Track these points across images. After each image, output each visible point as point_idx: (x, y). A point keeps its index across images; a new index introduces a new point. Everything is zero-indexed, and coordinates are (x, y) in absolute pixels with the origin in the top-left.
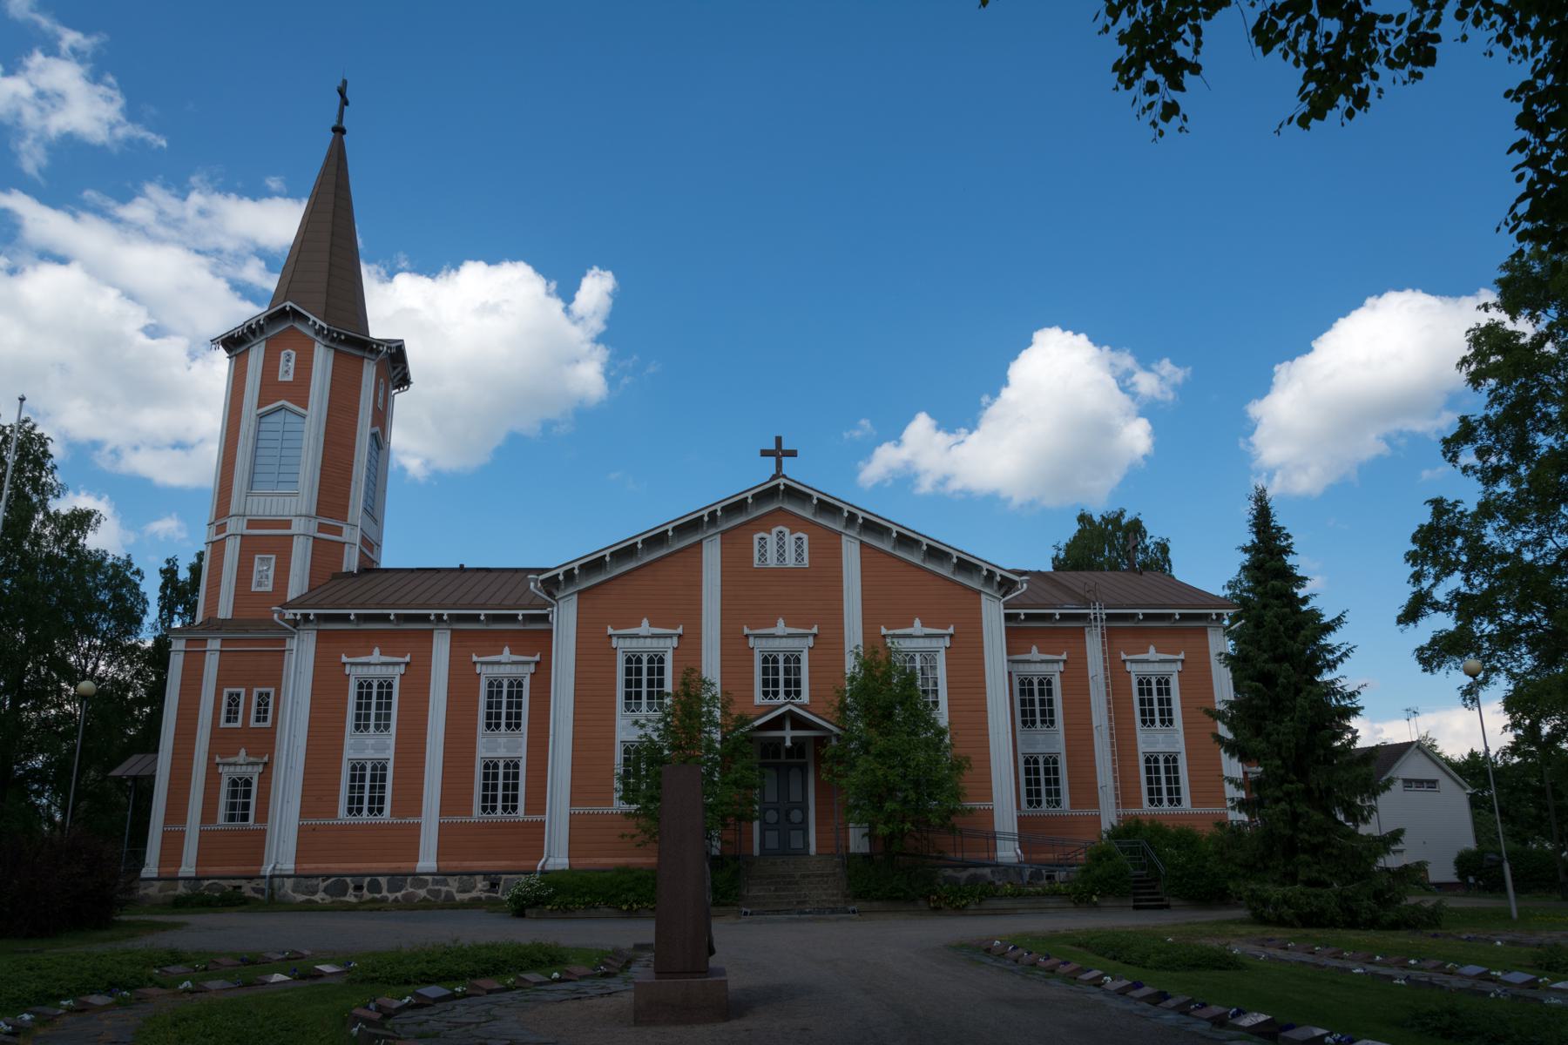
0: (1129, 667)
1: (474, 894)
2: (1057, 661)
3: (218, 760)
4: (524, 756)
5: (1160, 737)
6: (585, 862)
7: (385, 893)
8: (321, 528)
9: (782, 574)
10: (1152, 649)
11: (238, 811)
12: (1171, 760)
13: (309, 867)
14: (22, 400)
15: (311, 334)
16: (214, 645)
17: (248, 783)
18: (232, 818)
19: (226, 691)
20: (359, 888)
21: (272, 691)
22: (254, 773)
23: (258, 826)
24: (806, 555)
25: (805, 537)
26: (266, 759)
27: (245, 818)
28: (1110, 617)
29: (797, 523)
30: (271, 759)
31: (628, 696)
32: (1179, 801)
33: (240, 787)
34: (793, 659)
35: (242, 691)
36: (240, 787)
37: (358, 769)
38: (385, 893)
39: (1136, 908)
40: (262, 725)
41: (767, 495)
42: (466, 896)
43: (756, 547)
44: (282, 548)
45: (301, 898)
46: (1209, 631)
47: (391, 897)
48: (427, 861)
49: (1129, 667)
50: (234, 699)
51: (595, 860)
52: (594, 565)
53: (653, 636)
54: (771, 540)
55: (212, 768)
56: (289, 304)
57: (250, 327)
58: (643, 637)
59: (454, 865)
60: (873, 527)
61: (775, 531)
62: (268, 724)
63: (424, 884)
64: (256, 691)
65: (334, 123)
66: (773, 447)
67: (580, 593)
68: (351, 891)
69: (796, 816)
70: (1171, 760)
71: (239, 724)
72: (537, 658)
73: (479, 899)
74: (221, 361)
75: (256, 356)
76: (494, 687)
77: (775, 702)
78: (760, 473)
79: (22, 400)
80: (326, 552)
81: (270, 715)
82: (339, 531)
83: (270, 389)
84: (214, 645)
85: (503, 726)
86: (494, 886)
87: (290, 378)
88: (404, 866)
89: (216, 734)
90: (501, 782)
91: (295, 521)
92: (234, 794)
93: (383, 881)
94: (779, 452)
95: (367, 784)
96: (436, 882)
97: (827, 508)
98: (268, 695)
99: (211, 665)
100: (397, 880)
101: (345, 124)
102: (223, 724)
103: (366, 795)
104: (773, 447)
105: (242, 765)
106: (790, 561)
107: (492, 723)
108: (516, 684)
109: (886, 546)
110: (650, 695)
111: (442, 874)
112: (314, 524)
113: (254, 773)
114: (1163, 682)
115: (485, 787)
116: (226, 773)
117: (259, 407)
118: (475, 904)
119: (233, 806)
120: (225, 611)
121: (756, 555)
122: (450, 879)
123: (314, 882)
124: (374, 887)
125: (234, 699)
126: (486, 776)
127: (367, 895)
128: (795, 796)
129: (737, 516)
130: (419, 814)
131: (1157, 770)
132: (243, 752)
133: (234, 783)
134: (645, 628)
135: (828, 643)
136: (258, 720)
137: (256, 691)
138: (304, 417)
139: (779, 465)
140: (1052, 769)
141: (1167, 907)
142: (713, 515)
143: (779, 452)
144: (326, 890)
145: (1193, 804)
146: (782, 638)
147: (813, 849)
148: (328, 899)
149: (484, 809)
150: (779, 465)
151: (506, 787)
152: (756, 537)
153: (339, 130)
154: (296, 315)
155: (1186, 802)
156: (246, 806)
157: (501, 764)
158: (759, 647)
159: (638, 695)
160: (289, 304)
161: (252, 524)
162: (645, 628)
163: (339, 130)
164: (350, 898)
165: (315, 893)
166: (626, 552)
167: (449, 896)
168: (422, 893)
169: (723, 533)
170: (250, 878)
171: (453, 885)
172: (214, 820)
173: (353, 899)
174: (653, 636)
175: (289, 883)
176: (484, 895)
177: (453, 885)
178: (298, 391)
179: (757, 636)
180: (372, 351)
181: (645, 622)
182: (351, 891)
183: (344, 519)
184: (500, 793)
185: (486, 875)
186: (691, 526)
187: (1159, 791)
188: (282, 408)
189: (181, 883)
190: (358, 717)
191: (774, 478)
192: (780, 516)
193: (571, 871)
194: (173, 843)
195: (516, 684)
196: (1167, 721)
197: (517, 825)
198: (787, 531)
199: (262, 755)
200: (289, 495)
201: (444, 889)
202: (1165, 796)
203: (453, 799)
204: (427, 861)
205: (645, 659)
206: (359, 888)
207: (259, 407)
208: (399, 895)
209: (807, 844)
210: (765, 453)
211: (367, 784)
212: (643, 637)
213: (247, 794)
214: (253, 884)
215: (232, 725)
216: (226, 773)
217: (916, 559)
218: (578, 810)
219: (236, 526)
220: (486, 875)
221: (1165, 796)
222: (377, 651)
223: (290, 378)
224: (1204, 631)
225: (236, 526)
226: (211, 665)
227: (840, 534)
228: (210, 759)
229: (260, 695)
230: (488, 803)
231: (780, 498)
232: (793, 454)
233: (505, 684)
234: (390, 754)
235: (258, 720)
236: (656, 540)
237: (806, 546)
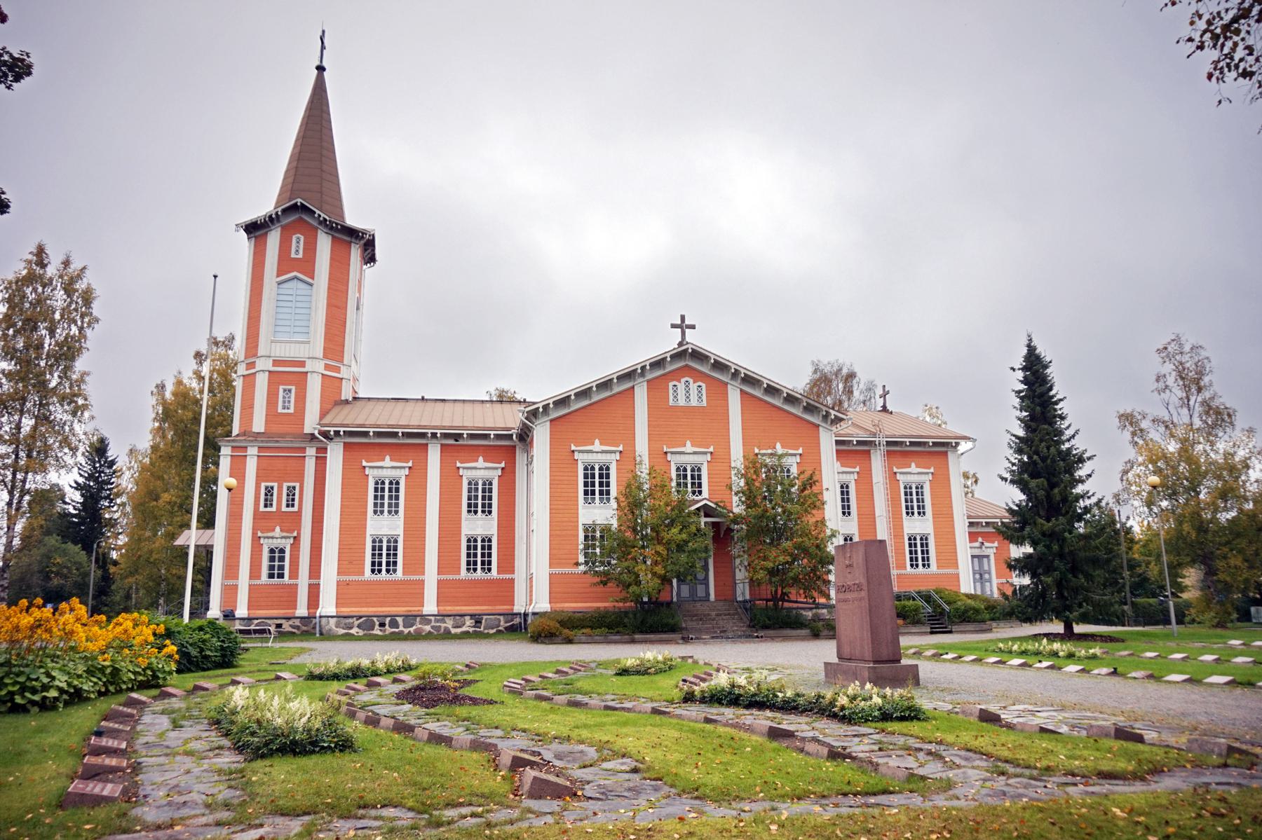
0: (577, 456)
1: (464, 629)
2: (614, 452)
3: (260, 534)
4: (401, 533)
5: (918, 524)
6: (559, 606)
7: (401, 628)
8: (327, 367)
9: (688, 410)
10: (913, 465)
11: (276, 572)
12: (924, 539)
13: (346, 610)
14: (215, 277)
15: (315, 224)
16: (253, 451)
17: (282, 551)
18: (271, 576)
19: (263, 485)
20: (382, 625)
21: (297, 485)
22: (287, 544)
23: (292, 581)
24: (704, 398)
25: (704, 386)
26: (295, 534)
27: (281, 576)
28: (888, 443)
29: (698, 376)
30: (299, 534)
31: (586, 493)
32: (490, 570)
33: (277, 555)
34: (697, 468)
35: (275, 485)
36: (277, 555)
37: (472, 541)
38: (401, 628)
39: (932, 633)
40: (290, 509)
41: (677, 356)
42: (459, 630)
43: (671, 391)
44: (300, 380)
45: (342, 631)
46: (950, 454)
47: (406, 631)
48: (430, 606)
49: (577, 456)
50: (269, 491)
51: (567, 605)
52: (563, 402)
53: (603, 452)
54: (681, 387)
55: (256, 540)
56: (299, 200)
57: (270, 217)
58: (596, 453)
59: (449, 609)
60: (750, 380)
61: (683, 380)
62: (296, 509)
63: (429, 622)
64: (285, 485)
65: (318, 63)
66: (679, 322)
67: (551, 421)
68: (377, 627)
69: (987, 576)
70: (924, 539)
71: (274, 509)
72: (503, 465)
73: (468, 632)
74: (243, 243)
75: (274, 239)
76: (472, 484)
77: (700, 497)
78: (669, 343)
79: (215, 277)
80: (331, 384)
81: (296, 503)
82: (338, 370)
83: (285, 263)
84: (253, 451)
85: (386, 513)
86: (478, 622)
87: (300, 256)
88: (414, 609)
89: (257, 515)
90: (479, 551)
91: (308, 363)
92: (272, 559)
93: (400, 620)
94: (682, 326)
95: (384, 552)
96: (437, 621)
97: (720, 366)
98: (294, 488)
99: (251, 466)
100: (410, 619)
101: (325, 64)
102: (262, 508)
103: (384, 560)
104: (679, 322)
105: (277, 538)
106: (694, 402)
107: (472, 509)
108: (488, 484)
109: (758, 393)
110: (601, 493)
111: (442, 616)
112: (322, 364)
113: (287, 544)
114: (920, 487)
115: (468, 555)
116: (266, 545)
117: (278, 276)
118: (466, 635)
119: (271, 568)
120: (259, 425)
121: (671, 397)
122: (447, 619)
123: (351, 620)
124: (394, 624)
125: (269, 491)
126: (469, 548)
127: (389, 630)
128: (986, 568)
129: (661, 371)
130: (513, 572)
131: (916, 545)
132: (278, 529)
133: (272, 551)
134: (597, 446)
135: (720, 458)
136: (288, 506)
137: (285, 485)
138: (311, 285)
139: (683, 334)
140: (925, 545)
141: (950, 632)
142: (643, 368)
143: (682, 326)
144: (359, 626)
145: (938, 567)
146: (689, 454)
147: (712, 597)
148: (361, 633)
149: (373, 571)
150: (683, 334)
151: (483, 555)
152: (671, 384)
153: (321, 69)
154: (304, 209)
155: (934, 567)
156: (281, 568)
157: (479, 540)
158: (675, 460)
159: (593, 493)
160: (299, 200)
161: (276, 363)
162: (597, 446)
163: (321, 69)
164: (377, 631)
165: (351, 628)
166: (584, 393)
167: (447, 632)
168: (428, 628)
169: (648, 381)
170: (288, 619)
171: (449, 623)
172: (259, 577)
173: (380, 633)
174: (603, 452)
175: (333, 621)
176: (471, 630)
177: (449, 623)
178: (307, 266)
179: (580, 452)
180: (357, 237)
181: (597, 442)
182: (377, 627)
183: (342, 361)
184: (479, 559)
185: (472, 616)
186: (629, 375)
187: (917, 559)
188: (296, 278)
189: (237, 622)
190: (375, 505)
191: (680, 344)
192: (687, 370)
193: (553, 612)
194: (230, 592)
195: (488, 484)
196: (922, 513)
197: (395, 582)
198: (691, 381)
199: (292, 531)
200: (302, 342)
201: (443, 625)
202: (920, 562)
203: (348, 560)
204: (430, 606)
205: (597, 467)
206: (382, 625)
207: (278, 276)
208: (412, 629)
209: (708, 594)
210: (674, 326)
211: (384, 552)
212: (596, 453)
213: (282, 559)
214: (291, 622)
215: (268, 509)
216: (266, 545)
217: (778, 402)
218: (557, 570)
219: (263, 364)
220: (472, 616)
221: (920, 562)
222: (388, 458)
223: (300, 256)
224: (945, 454)
225: (263, 364)
226: (251, 466)
227: (727, 384)
228: (254, 534)
229: (288, 488)
230: (471, 566)
231: (689, 359)
232: (693, 327)
233: (480, 483)
234: (400, 531)
235: (288, 506)
236: (605, 385)
237: (704, 392)
